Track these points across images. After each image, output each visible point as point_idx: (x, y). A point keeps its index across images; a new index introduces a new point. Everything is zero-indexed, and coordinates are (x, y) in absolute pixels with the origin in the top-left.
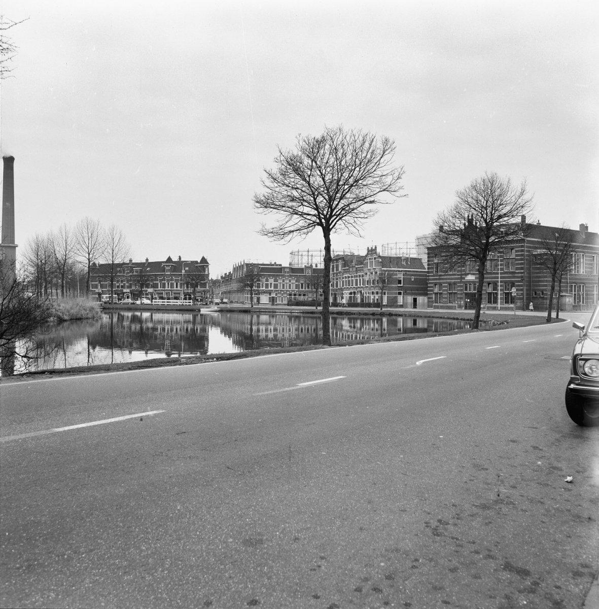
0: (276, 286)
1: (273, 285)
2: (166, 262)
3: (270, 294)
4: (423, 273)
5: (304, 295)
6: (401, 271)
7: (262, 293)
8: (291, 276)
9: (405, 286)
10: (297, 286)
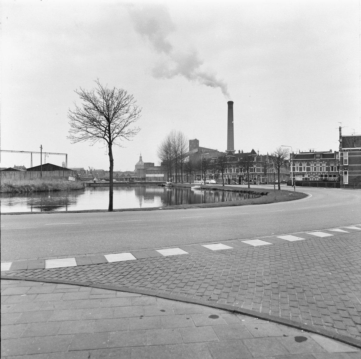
0: (308, 169)
1: (299, 168)
2: (251, 153)
3: (303, 176)
4: (321, 153)
5: (335, 176)
6: (347, 151)
7: (297, 175)
8: (321, 161)
9: (349, 165)
10: (328, 169)
